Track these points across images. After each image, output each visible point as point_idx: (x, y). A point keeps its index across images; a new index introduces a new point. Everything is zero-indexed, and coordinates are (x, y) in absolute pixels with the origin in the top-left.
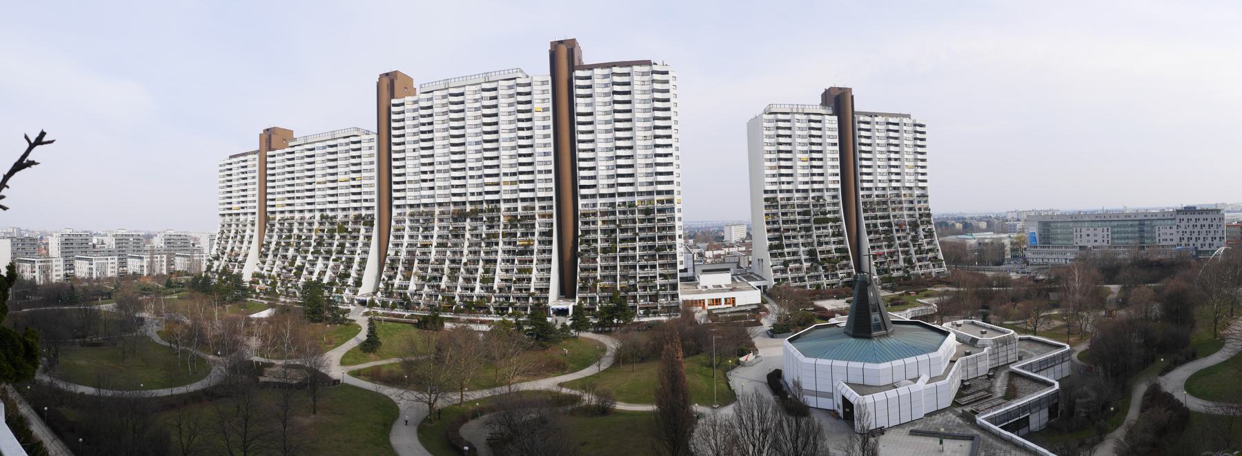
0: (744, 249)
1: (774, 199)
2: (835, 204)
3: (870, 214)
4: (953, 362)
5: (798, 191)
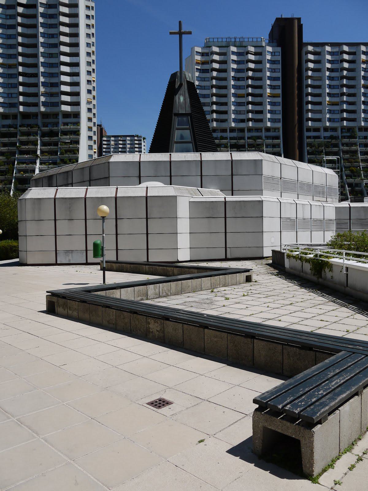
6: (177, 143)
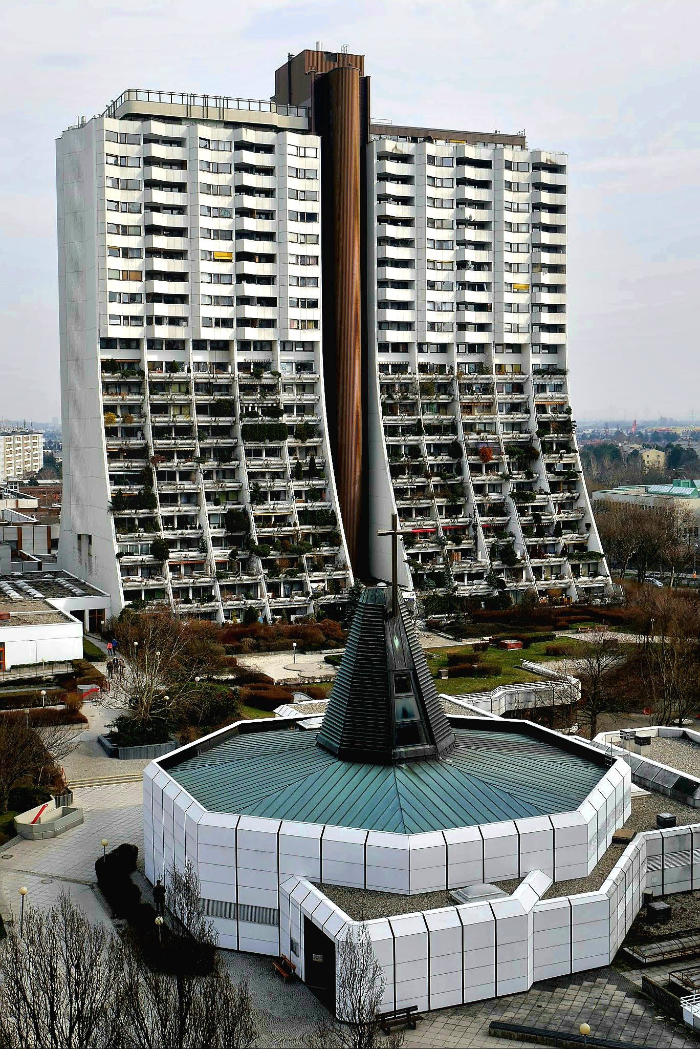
0: (33, 503)
1: (133, 366)
2: (303, 388)
3: (401, 419)
4: (620, 842)
5: (199, 345)
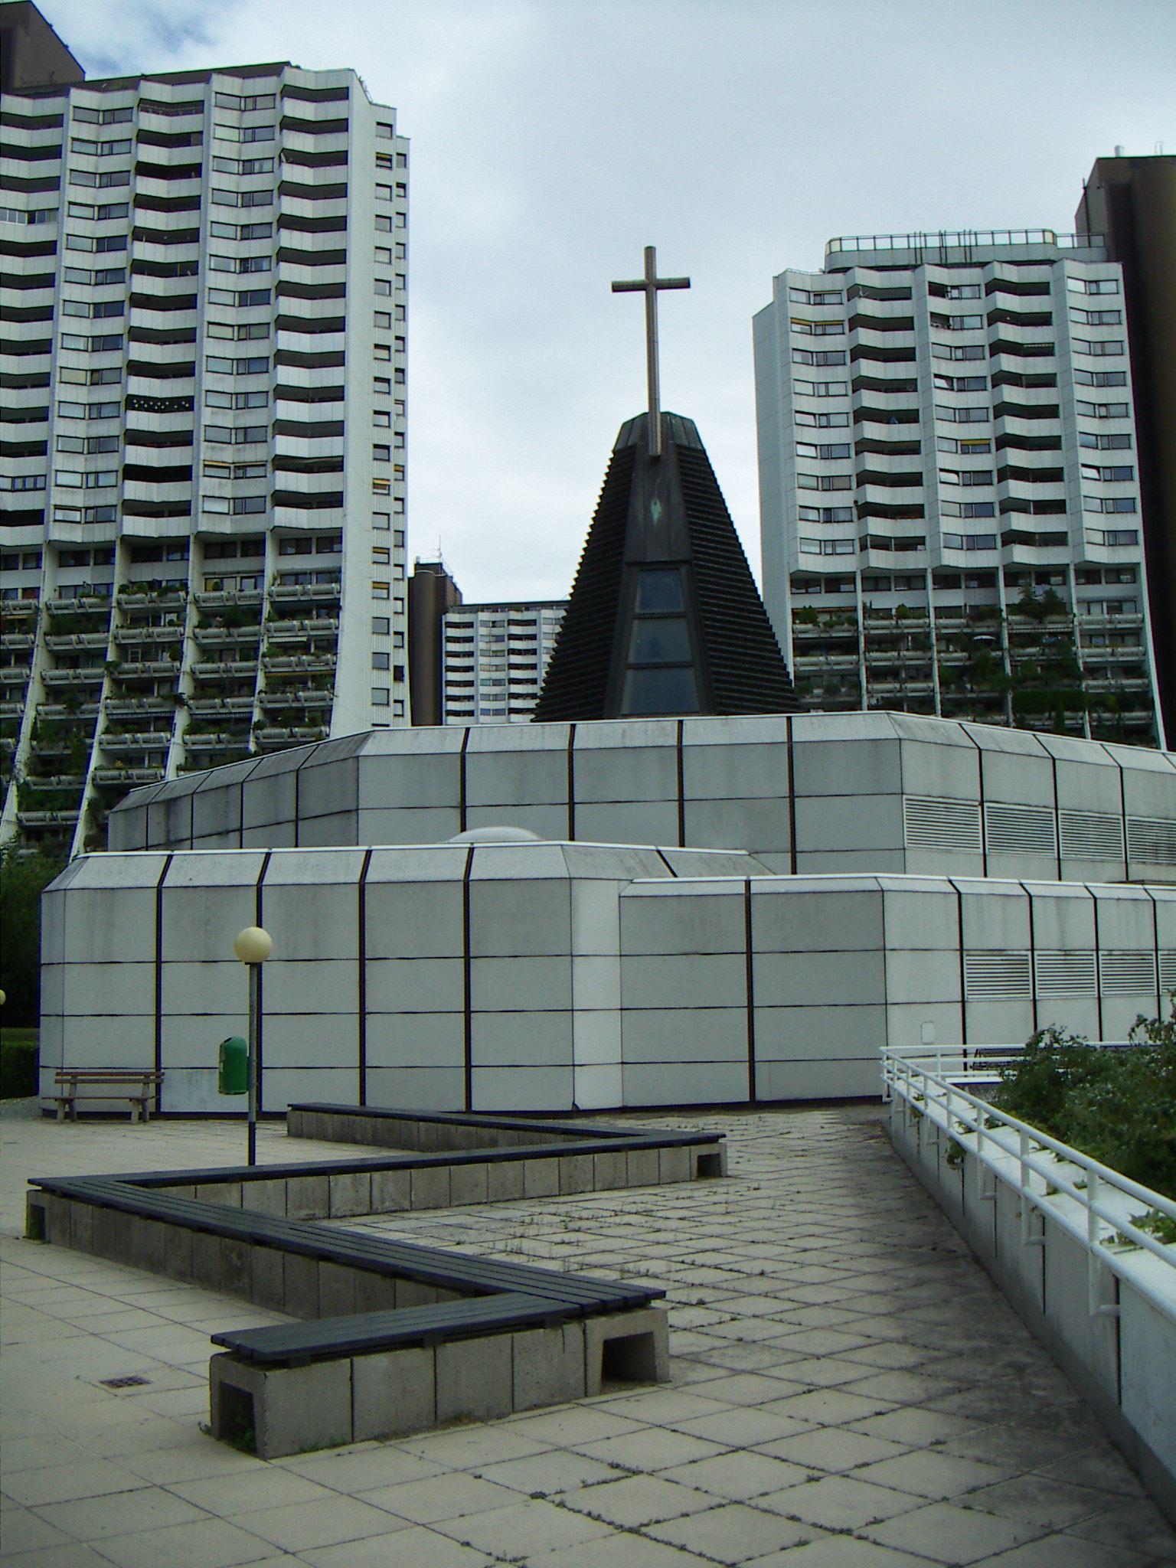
5: (948, 578)
6: (638, 667)
